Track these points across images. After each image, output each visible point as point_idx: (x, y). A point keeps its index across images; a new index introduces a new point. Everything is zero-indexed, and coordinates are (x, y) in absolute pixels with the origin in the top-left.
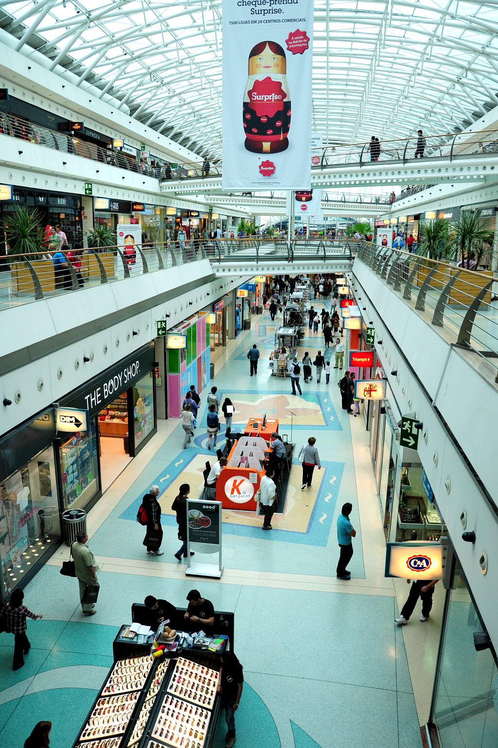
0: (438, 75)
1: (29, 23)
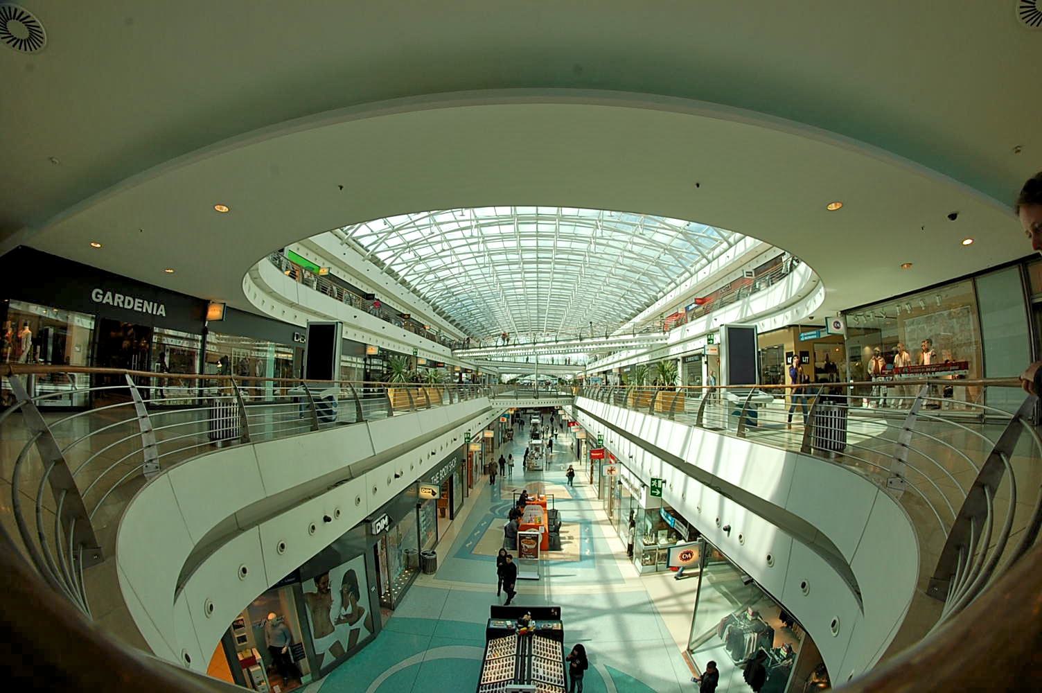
0: (612, 293)
1: (388, 262)
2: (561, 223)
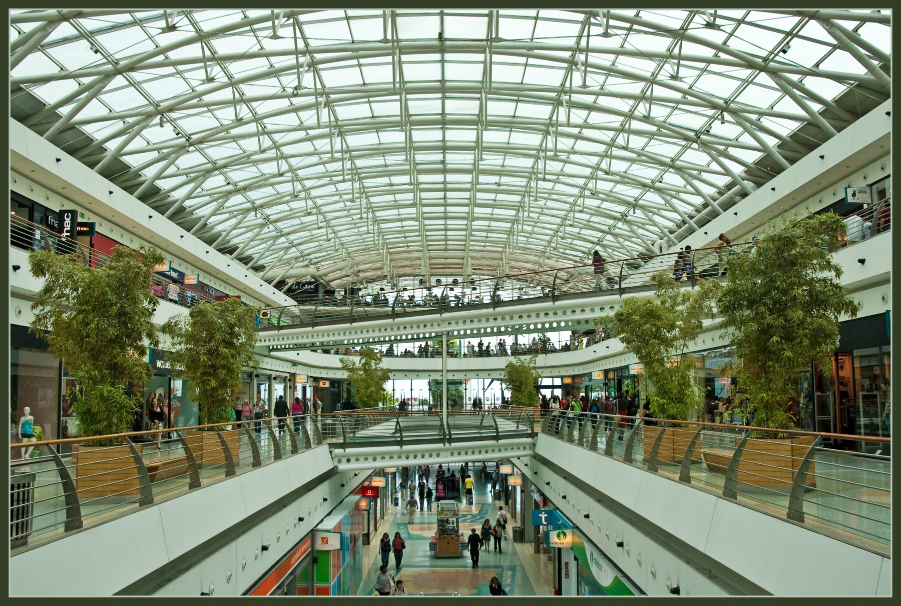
2: (489, 96)
